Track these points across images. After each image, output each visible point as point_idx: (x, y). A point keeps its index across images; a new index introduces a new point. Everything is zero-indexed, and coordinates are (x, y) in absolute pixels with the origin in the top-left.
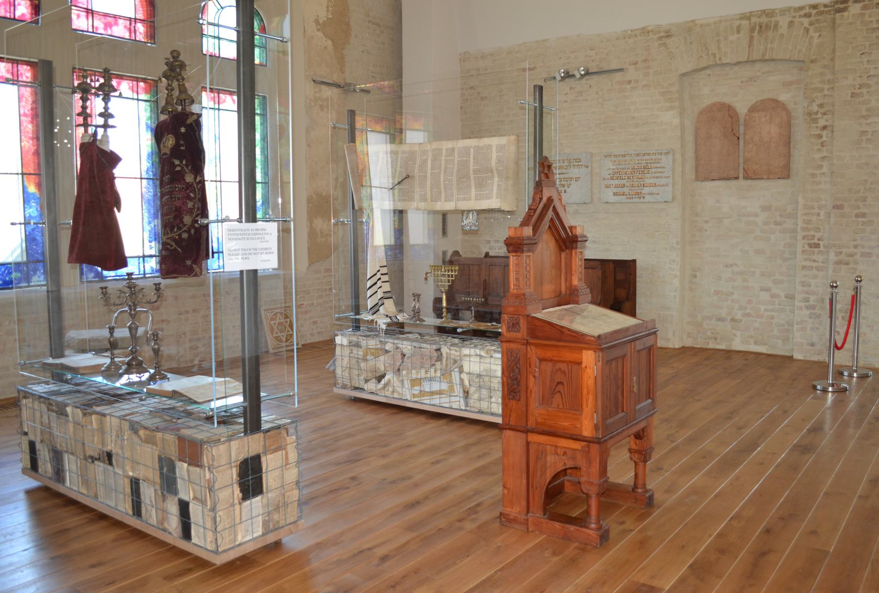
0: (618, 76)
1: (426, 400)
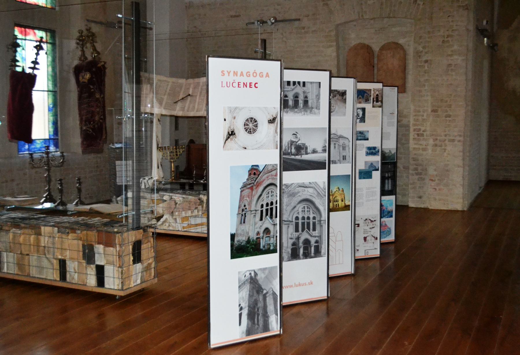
0: (297, 23)
1: (193, 230)
